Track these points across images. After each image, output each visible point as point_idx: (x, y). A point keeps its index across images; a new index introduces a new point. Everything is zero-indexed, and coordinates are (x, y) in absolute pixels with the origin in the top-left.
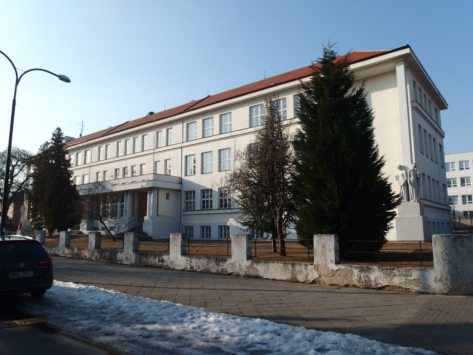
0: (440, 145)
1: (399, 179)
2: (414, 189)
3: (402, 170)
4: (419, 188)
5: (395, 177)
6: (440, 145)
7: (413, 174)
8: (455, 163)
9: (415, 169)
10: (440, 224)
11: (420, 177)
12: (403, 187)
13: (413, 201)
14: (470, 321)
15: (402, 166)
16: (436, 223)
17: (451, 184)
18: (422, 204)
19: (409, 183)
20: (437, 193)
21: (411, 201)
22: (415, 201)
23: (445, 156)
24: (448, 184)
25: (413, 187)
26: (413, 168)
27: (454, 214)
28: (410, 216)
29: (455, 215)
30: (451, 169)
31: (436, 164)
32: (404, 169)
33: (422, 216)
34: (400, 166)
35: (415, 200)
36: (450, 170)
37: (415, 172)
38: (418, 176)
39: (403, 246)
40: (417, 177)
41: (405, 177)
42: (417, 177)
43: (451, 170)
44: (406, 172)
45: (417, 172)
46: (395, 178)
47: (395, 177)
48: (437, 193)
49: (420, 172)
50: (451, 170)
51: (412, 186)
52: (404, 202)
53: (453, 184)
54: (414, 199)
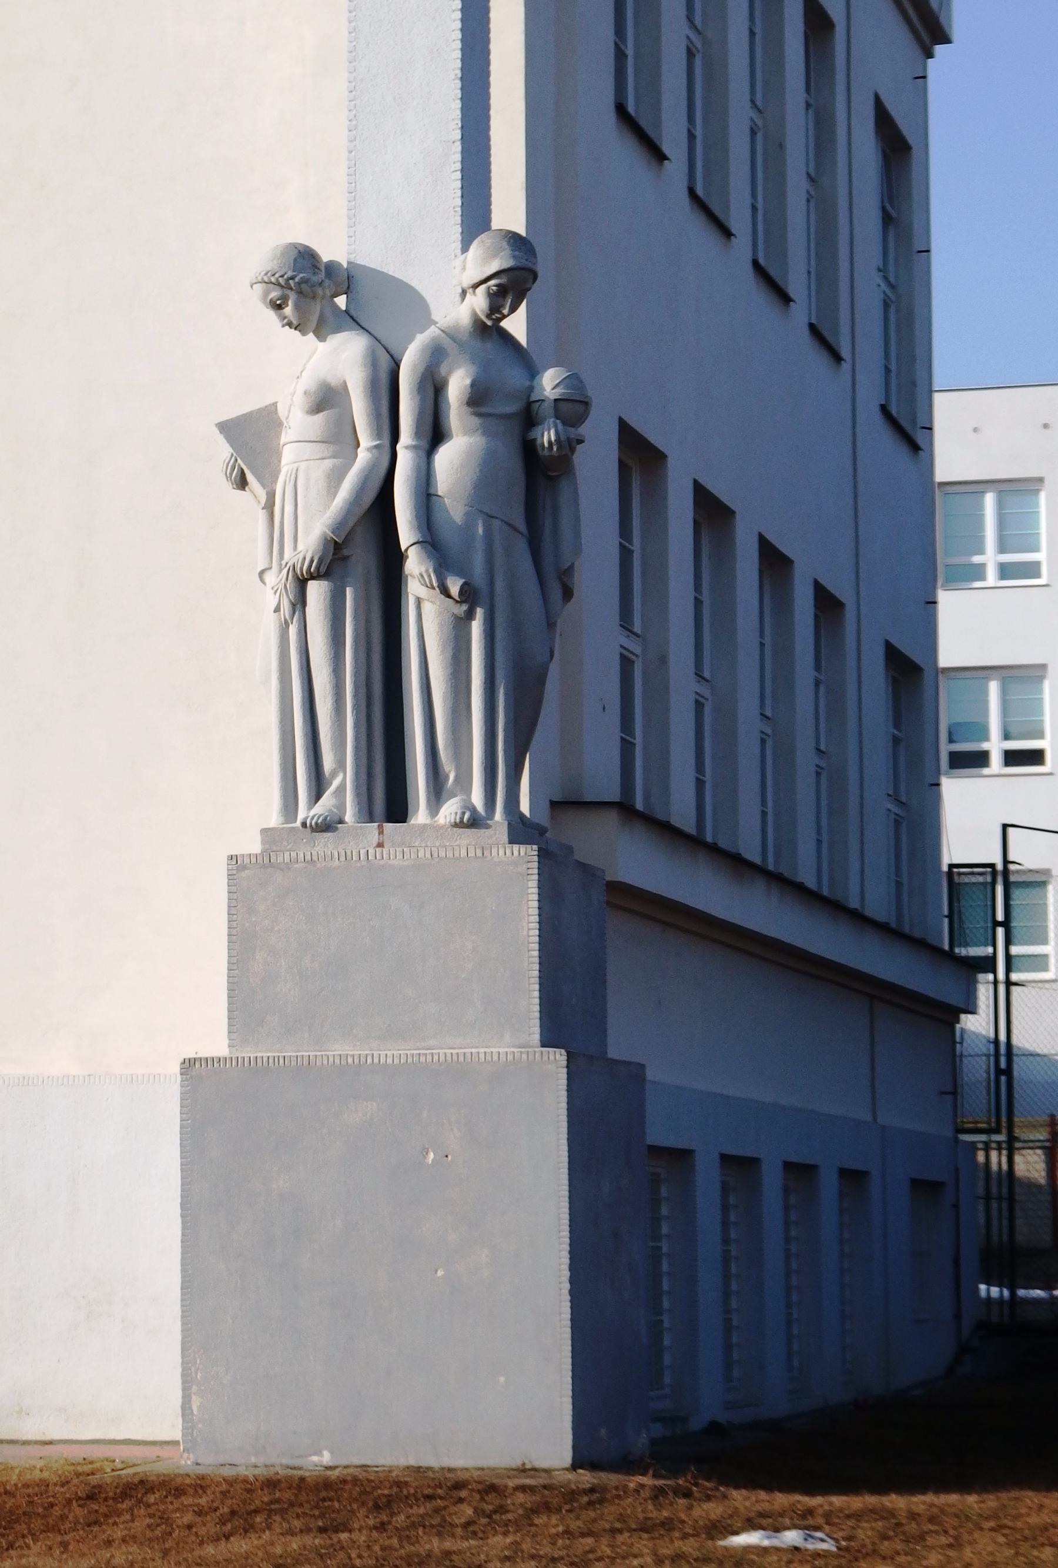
0: (892, 654)
1: (269, 475)
2: (477, 627)
3: (321, 334)
4: (551, 625)
5: (227, 428)
6: (892, 654)
7: (477, 399)
8: (1043, 496)
9: (516, 324)
10: (829, 1183)
11: (569, 445)
12: (317, 591)
13: (450, 811)
14: (458, 4)
15: (331, 268)
16: (772, 1178)
17: (987, 738)
18: (585, 868)
19: (406, 533)
20: (805, 759)
21: (420, 816)
22: (474, 822)
23: (938, 398)
24: (951, 741)
25: (469, 596)
26: (479, 301)
27: (999, 1072)
28: (391, 1053)
29: (1008, 1072)
30: (990, 558)
31: (816, 360)
32: (352, 320)
33: (559, 1056)
34: (305, 257)
35: (477, 798)
36: (978, 572)
37: (514, 377)
38: (547, 435)
39: (248, 1529)
40: (529, 450)
41: (366, 441)
42: (529, 450)
43: (991, 576)
44: (373, 364)
45: (533, 372)
46: (224, 450)
47: (227, 428)
48: (805, 759)
49: (573, 381)
50: (991, 576)
51: (455, 586)
52: (327, 826)
53: (1007, 736)
54: (464, 782)
